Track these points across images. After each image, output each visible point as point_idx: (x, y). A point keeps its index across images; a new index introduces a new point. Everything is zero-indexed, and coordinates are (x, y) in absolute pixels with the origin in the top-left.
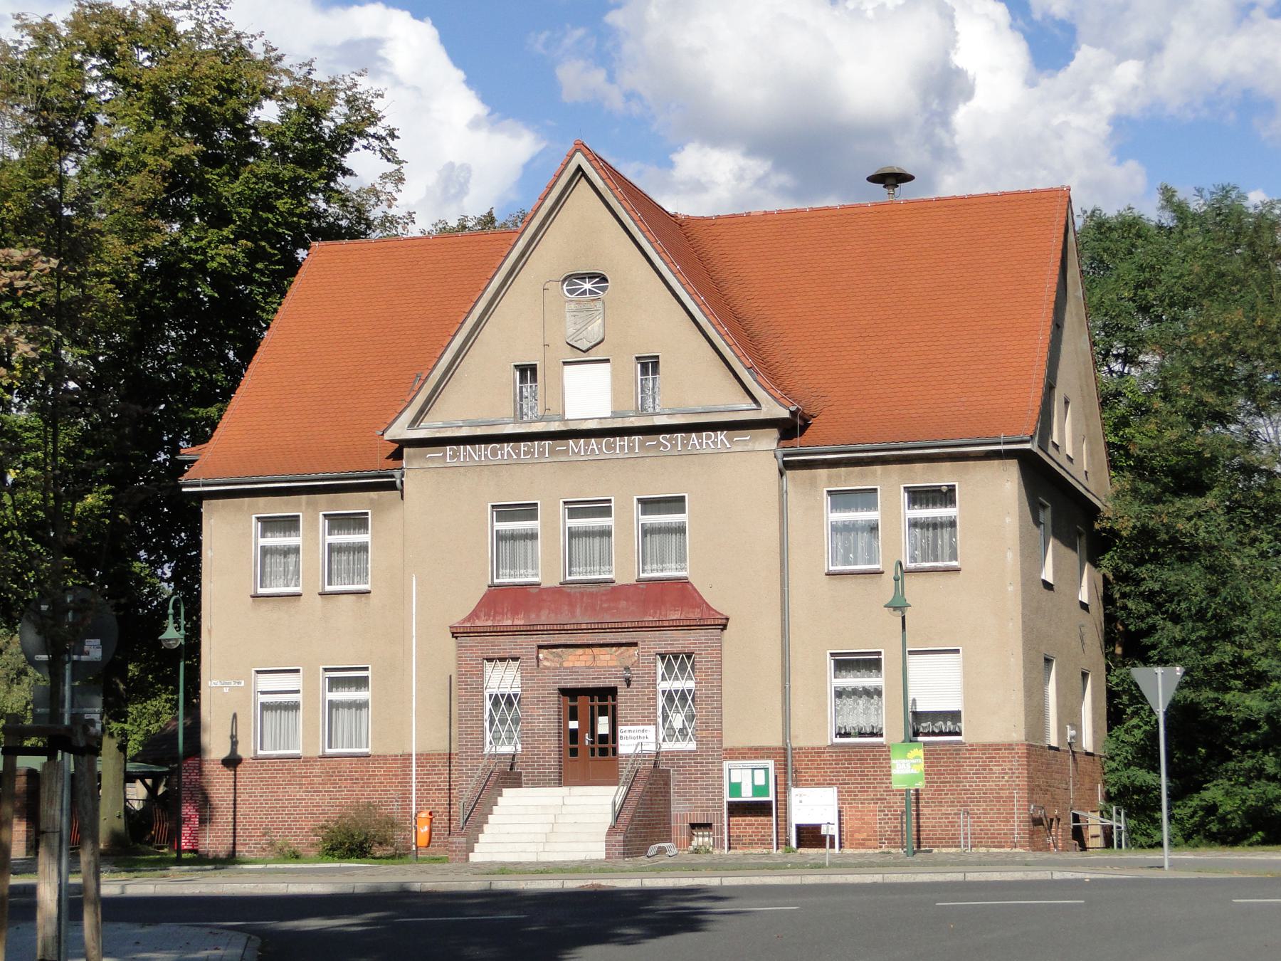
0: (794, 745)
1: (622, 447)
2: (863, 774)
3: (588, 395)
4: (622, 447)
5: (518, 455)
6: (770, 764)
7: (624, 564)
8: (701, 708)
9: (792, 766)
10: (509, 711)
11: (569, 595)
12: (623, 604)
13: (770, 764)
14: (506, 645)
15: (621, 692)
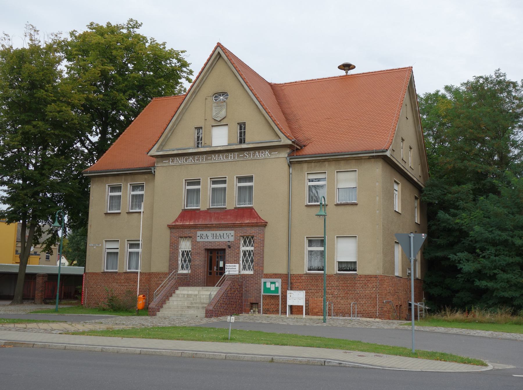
0: (292, 273)
1: (231, 157)
2: (317, 286)
3: (220, 138)
4: (231, 157)
5: (194, 161)
6: (280, 280)
7: (232, 202)
8: (254, 259)
9: (290, 282)
10: (250, 257)
11: (210, 213)
12: (229, 217)
13: (280, 280)
14: (187, 232)
15: (227, 251)
